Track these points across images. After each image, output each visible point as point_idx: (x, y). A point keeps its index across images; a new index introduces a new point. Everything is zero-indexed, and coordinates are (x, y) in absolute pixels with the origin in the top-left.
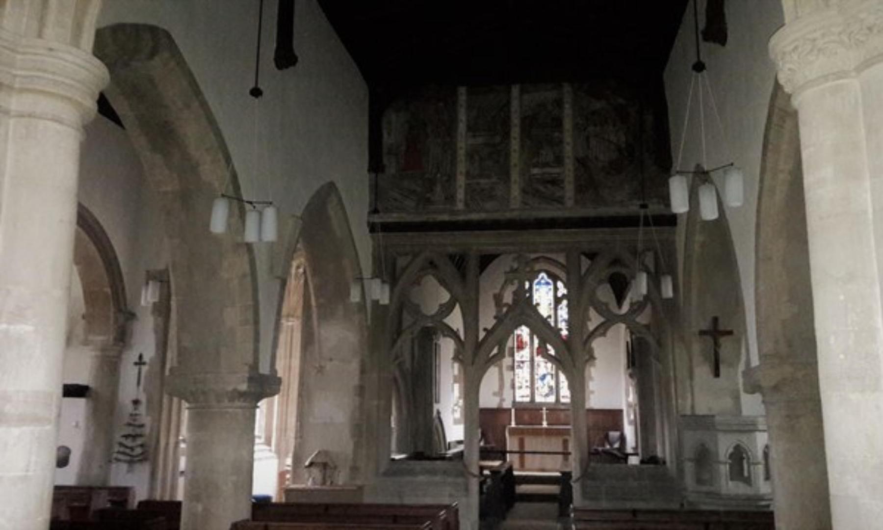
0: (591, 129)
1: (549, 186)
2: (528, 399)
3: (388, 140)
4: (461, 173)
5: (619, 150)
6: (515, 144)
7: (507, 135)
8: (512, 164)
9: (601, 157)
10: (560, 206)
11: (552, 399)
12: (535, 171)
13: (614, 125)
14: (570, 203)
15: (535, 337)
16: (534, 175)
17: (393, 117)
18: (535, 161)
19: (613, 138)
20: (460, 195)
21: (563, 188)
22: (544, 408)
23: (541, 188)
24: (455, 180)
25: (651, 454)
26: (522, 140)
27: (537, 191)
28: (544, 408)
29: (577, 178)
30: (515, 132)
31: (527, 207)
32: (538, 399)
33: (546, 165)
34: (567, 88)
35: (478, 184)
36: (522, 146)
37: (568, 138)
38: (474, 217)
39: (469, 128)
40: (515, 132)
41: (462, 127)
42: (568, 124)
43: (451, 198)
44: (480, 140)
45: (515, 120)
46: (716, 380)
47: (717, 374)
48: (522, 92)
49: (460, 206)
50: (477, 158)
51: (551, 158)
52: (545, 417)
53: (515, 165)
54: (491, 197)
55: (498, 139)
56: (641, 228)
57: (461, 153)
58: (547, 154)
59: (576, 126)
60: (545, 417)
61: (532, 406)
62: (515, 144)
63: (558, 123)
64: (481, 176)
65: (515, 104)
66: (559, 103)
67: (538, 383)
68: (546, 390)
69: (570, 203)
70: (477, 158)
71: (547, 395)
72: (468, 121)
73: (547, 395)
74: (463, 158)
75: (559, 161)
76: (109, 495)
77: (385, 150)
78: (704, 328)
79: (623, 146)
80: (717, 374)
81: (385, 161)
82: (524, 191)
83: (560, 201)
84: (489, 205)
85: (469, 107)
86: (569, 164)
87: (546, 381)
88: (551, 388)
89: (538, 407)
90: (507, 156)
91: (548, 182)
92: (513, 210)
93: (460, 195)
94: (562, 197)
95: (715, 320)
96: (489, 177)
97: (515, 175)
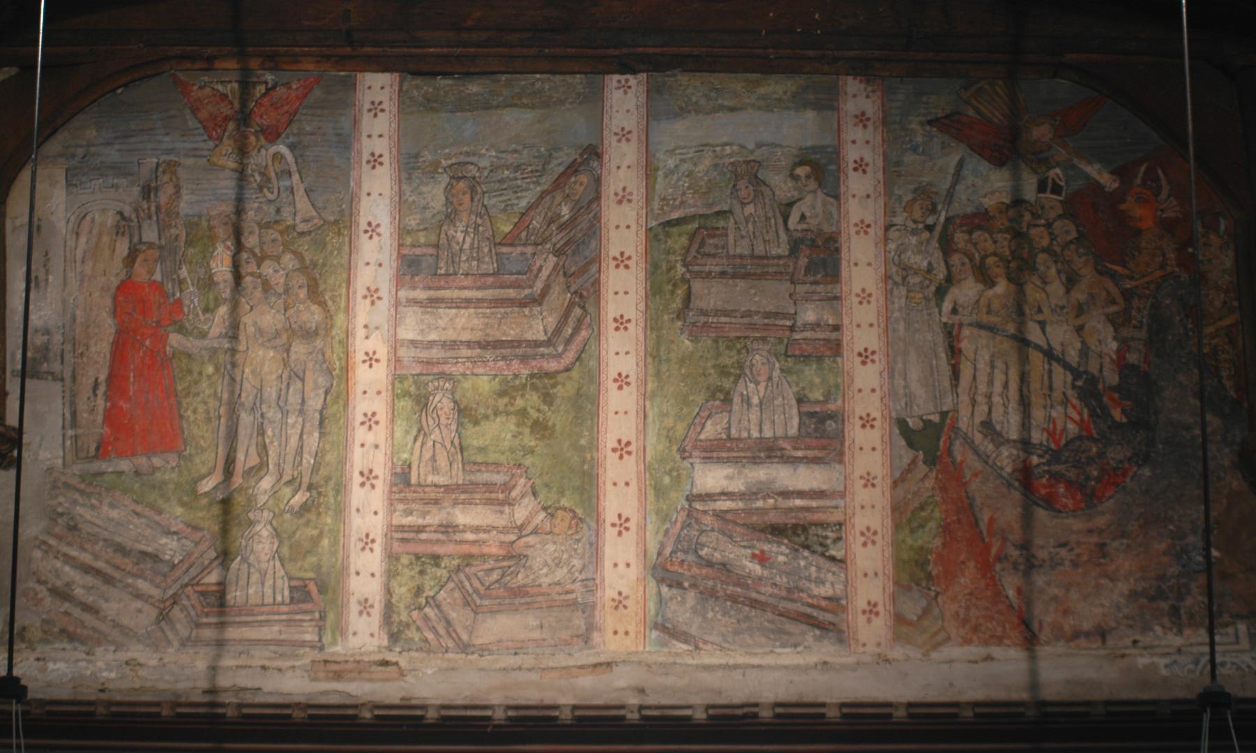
0: (967, 291)
1: (780, 552)
5: (1089, 390)
6: (621, 353)
7: (585, 297)
8: (609, 440)
12: (712, 478)
13: (1071, 282)
14: (872, 632)
16: (708, 497)
17: (56, 202)
18: (711, 430)
19: (1060, 335)
24: (340, 511)
26: (653, 323)
29: (904, 516)
35: (448, 528)
36: (655, 354)
37: (863, 327)
39: (410, 267)
42: (862, 265)
48: (653, 113)
50: (442, 403)
53: (622, 524)
54: (519, 597)
55: (537, 326)
57: (370, 383)
59: (897, 275)
62: (621, 353)
64: (463, 492)
66: (822, 168)
70: (442, 403)
72: (403, 232)
74: (379, 406)
75: (822, 433)
76: (403, 286)
79: (1111, 377)
82: (664, 573)
84: (500, 626)
85: (410, 166)
86: (870, 451)
90: (586, 406)
91: (777, 531)
96: (499, 497)
97: (621, 493)
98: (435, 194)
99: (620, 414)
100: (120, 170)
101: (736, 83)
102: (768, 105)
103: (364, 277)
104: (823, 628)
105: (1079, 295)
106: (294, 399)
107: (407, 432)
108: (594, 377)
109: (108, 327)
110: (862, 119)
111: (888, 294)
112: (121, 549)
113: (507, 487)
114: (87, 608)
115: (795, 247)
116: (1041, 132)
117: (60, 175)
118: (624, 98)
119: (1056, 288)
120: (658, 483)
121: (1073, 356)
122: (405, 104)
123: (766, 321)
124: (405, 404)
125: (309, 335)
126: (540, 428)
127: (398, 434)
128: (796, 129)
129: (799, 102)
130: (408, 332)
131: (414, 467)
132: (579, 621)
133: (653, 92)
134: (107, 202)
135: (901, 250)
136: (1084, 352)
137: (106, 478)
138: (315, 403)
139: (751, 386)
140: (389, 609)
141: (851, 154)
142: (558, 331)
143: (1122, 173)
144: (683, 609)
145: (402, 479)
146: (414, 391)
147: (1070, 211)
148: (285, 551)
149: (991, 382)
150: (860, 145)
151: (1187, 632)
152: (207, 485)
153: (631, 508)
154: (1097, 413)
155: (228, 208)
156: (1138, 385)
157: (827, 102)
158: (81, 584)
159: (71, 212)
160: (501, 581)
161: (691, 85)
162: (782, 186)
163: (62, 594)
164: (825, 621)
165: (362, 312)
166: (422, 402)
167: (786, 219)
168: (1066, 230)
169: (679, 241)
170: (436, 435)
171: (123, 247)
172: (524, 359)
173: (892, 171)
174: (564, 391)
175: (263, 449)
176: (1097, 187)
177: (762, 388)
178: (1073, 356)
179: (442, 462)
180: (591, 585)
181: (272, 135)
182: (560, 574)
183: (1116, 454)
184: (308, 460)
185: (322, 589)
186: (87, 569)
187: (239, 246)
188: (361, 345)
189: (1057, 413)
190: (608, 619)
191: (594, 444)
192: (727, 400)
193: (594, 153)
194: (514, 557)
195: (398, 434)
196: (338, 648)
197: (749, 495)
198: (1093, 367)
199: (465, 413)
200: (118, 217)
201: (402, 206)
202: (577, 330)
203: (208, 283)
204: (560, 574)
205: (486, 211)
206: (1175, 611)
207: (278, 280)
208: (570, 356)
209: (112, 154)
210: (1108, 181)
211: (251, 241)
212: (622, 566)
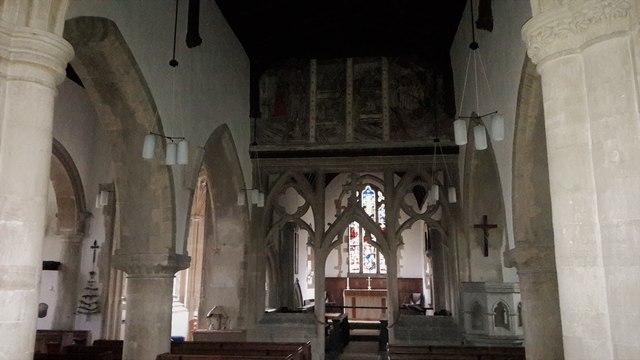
2: (358, 271)
5: (420, 102)
11: (374, 271)
12: (363, 116)
14: (386, 139)
20: (312, 132)
23: (367, 128)
27: (364, 130)
29: (391, 121)
30: (350, 90)
32: (365, 271)
33: (371, 112)
34: (385, 60)
37: (385, 93)
39: (318, 88)
40: (350, 90)
41: (313, 87)
42: (385, 85)
43: (306, 135)
44: (326, 96)
45: (350, 81)
47: (486, 254)
48: (354, 63)
49: (312, 140)
51: (373, 108)
57: (313, 105)
62: (349, 98)
63: (379, 84)
66: (379, 71)
67: (365, 261)
68: (370, 265)
69: (386, 139)
75: (379, 110)
77: (261, 102)
80: (486, 254)
83: (380, 137)
84: (331, 140)
85: (318, 73)
86: (386, 112)
93: (312, 132)
95: (485, 217)
97: (349, 119)
99: (349, 108)
123: (600, 260)
128: (374, 65)
130: (319, 97)
137: (450, 306)
145: (317, 119)
146: (319, 106)
150: (385, 68)
159: (566, 358)
160: (331, 133)
162: (373, 74)
193: (345, 70)
194: (334, 129)
212: (350, 130)
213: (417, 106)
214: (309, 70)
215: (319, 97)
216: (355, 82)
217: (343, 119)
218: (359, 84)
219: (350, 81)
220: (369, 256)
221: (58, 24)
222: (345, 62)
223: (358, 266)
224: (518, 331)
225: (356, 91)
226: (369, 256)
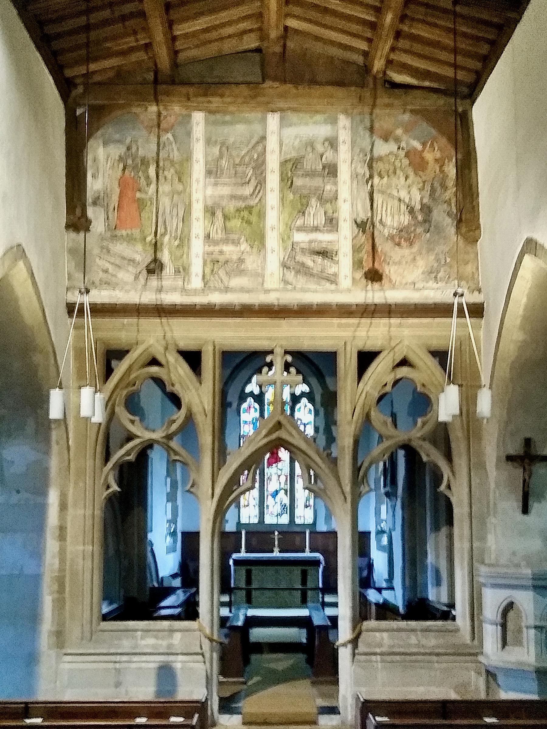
1: (319, 259)
2: (256, 521)
3: (94, 185)
4: (197, 237)
5: (411, 211)
7: (261, 183)
9: (388, 221)
10: (333, 287)
11: (285, 520)
12: (300, 237)
13: (407, 178)
14: (345, 282)
15: (297, 464)
18: (299, 222)
19: (403, 194)
20: (197, 267)
21: (337, 262)
22: (276, 533)
23: (309, 262)
25: (419, 595)
26: (281, 191)
27: (303, 264)
28: (276, 533)
30: (273, 180)
31: (289, 287)
32: (269, 520)
33: (316, 229)
34: (343, 121)
35: (221, 252)
38: (216, 298)
40: (273, 180)
41: (198, 169)
42: (344, 172)
43: (183, 271)
44: (226, 191)
45: (273, 163)
46: (525, 517)
47: (525, 510)
48: (283, 123)
49: (196, 283)
50: (219, 214)
51: (321, 220)
52: (276, 543)
54: (242, 272)
55: (247, 191)
56: (454, 320)
58: (315, 214)
60: (276, 543)
61: (260, 529)
63: (331, 171)
64: (226, 241)
65: (272, 143)
67: (269, 501)
68: (278, 509)
69: (345, 282)
70: (219, 214)
71: (279, 515)
73: (279, 515)
75: (332, 223)
77: (89, 200)
78: (512, 452)
79: (418, 207)
80: (525, 510)
81: (90, 212)
82: (285, 266)
83: (333, 279)
84: (236, 282)
87: (278, 498)
88: (284, 507)
89: (268, 529)
91: (318, 253)
92: (267, 291)
93: (197, 267)
94: (335, 275)
95: (528, 442)
96: (236, 243)
97: (272, 240)
98: (216, 150)
100: (119, 141)
101: (306, 117)
102: (315, 123)
103: (195, 176)
104: (332, 282)
105: (409, 181)
106: (175, 213)
107: (209, 222)
108: (264, 206)
109: (118, 190)
110: (344, 128)
111: (352, 182)
112: (123, 258)
113: (239, 239)
114: (113, 275)
115: (324, 168)
116: (399, 132)
117: (101, 142)
118: (273, 120)
119: (402, 179)
120: (284, 239)
121: (407, 200)
122: (207, 121)
124: (208, 215)
125: (179, 193)
126: (249, 222)
127: (206, 224)
129: (326, 122)
131: (360, 696)
132: (260, 280)
133: (282, 119)
134: (116, 151)
135: (355, 168)
136: (410, 199)
138: (181, 214)
139: (311, 208)
140: (204, 276)
141: (341, 139)
142: (253, 192)
143: (424, 144)
144: (290, 276)
147: (407, 155)
148: (173, 258)
149: (382, 207)
150: (344, 136)
151: (440, 283)
152: (149, 239)
153: (276, 248)
154: (414, 217)
155: (155, 155)
156: (426, 210)
157: (334, 121)
158: (111, 268)
160: (238, 267)
161: (293, 117)
162: (320, 148)
163: (106, 271)
164: (333, 279)
165: (194, 186)
166: (213, 214)
167: (321, 160)
168: (406, 162)
169: (289, 165)
170: (217, 223)
171: (121, 166)
172: (244, 201)
173: (353, 143)
174: (255, 211)
175: (166, 229)
176: (416, 149)
177: (314, 209)
178: (407, 200)
179: (219, 231)
180: (263, 269)
181: (167, 131)
182: (255, 265)
183: (419, 230)
184: (179, 232)
185: (184, 269)
186: (112, 264)
187: (158, 166)
188: (194, 197)
189: (402, 217)
190: (267, 278)
191: (264, 227)
192: (304, 213)
193: (263, 138)
194: (241, 261)
195: (206, 224)
196: (189, 286)
197: (310, 242)
198: (413, 203)
199: (226, 218)
200: (365, 315)
201: (206, 155)
202: (259, 192)
203: (148, 178)
204: (255, 265)
205: (231, 155)
206: (436, 277)
207: (169, 177)
208: (258, 199)
209: (117, 136)
210: (419, 147)
211: (161, 164)
213: (406, 219)
214: (189, 134)
215: (210, 191)
216: (283, 163)
217: (258, 239)
218: (291, 167)
219: (273, 163)
220: (277, 492)
221: (227, 474)
222: (264, 120)
223: (256, 511)
224: (432, 458)
225: (287, 182)
226: (277, 492)
